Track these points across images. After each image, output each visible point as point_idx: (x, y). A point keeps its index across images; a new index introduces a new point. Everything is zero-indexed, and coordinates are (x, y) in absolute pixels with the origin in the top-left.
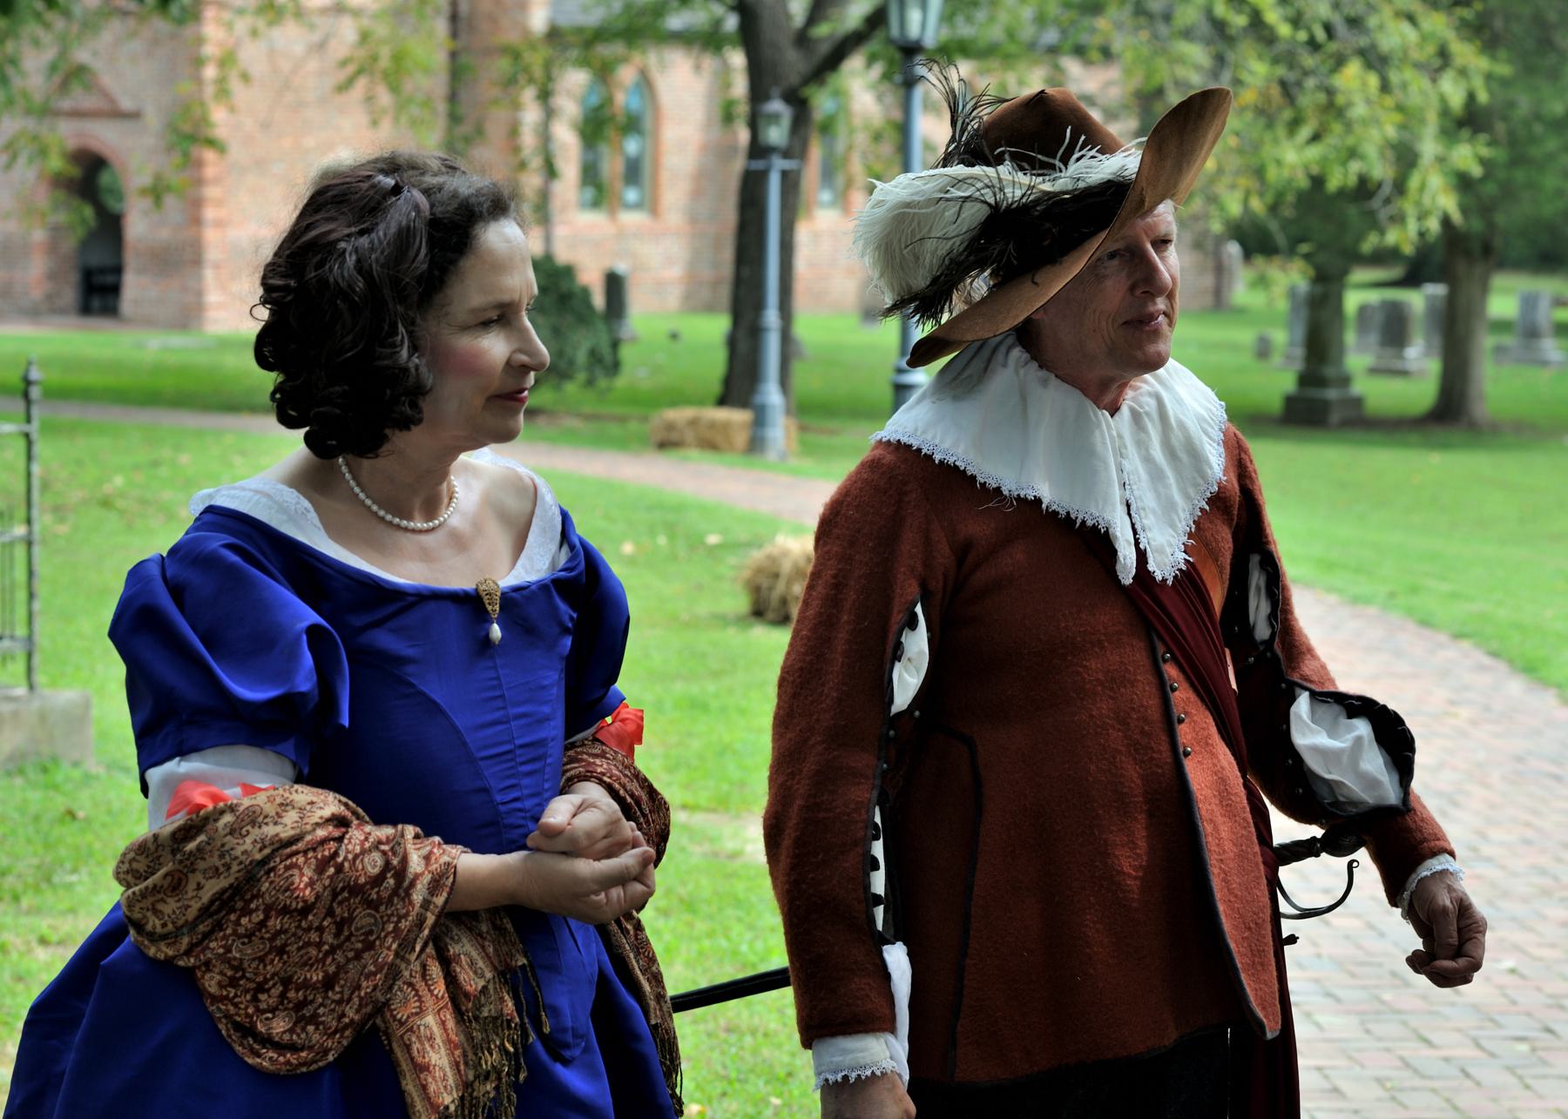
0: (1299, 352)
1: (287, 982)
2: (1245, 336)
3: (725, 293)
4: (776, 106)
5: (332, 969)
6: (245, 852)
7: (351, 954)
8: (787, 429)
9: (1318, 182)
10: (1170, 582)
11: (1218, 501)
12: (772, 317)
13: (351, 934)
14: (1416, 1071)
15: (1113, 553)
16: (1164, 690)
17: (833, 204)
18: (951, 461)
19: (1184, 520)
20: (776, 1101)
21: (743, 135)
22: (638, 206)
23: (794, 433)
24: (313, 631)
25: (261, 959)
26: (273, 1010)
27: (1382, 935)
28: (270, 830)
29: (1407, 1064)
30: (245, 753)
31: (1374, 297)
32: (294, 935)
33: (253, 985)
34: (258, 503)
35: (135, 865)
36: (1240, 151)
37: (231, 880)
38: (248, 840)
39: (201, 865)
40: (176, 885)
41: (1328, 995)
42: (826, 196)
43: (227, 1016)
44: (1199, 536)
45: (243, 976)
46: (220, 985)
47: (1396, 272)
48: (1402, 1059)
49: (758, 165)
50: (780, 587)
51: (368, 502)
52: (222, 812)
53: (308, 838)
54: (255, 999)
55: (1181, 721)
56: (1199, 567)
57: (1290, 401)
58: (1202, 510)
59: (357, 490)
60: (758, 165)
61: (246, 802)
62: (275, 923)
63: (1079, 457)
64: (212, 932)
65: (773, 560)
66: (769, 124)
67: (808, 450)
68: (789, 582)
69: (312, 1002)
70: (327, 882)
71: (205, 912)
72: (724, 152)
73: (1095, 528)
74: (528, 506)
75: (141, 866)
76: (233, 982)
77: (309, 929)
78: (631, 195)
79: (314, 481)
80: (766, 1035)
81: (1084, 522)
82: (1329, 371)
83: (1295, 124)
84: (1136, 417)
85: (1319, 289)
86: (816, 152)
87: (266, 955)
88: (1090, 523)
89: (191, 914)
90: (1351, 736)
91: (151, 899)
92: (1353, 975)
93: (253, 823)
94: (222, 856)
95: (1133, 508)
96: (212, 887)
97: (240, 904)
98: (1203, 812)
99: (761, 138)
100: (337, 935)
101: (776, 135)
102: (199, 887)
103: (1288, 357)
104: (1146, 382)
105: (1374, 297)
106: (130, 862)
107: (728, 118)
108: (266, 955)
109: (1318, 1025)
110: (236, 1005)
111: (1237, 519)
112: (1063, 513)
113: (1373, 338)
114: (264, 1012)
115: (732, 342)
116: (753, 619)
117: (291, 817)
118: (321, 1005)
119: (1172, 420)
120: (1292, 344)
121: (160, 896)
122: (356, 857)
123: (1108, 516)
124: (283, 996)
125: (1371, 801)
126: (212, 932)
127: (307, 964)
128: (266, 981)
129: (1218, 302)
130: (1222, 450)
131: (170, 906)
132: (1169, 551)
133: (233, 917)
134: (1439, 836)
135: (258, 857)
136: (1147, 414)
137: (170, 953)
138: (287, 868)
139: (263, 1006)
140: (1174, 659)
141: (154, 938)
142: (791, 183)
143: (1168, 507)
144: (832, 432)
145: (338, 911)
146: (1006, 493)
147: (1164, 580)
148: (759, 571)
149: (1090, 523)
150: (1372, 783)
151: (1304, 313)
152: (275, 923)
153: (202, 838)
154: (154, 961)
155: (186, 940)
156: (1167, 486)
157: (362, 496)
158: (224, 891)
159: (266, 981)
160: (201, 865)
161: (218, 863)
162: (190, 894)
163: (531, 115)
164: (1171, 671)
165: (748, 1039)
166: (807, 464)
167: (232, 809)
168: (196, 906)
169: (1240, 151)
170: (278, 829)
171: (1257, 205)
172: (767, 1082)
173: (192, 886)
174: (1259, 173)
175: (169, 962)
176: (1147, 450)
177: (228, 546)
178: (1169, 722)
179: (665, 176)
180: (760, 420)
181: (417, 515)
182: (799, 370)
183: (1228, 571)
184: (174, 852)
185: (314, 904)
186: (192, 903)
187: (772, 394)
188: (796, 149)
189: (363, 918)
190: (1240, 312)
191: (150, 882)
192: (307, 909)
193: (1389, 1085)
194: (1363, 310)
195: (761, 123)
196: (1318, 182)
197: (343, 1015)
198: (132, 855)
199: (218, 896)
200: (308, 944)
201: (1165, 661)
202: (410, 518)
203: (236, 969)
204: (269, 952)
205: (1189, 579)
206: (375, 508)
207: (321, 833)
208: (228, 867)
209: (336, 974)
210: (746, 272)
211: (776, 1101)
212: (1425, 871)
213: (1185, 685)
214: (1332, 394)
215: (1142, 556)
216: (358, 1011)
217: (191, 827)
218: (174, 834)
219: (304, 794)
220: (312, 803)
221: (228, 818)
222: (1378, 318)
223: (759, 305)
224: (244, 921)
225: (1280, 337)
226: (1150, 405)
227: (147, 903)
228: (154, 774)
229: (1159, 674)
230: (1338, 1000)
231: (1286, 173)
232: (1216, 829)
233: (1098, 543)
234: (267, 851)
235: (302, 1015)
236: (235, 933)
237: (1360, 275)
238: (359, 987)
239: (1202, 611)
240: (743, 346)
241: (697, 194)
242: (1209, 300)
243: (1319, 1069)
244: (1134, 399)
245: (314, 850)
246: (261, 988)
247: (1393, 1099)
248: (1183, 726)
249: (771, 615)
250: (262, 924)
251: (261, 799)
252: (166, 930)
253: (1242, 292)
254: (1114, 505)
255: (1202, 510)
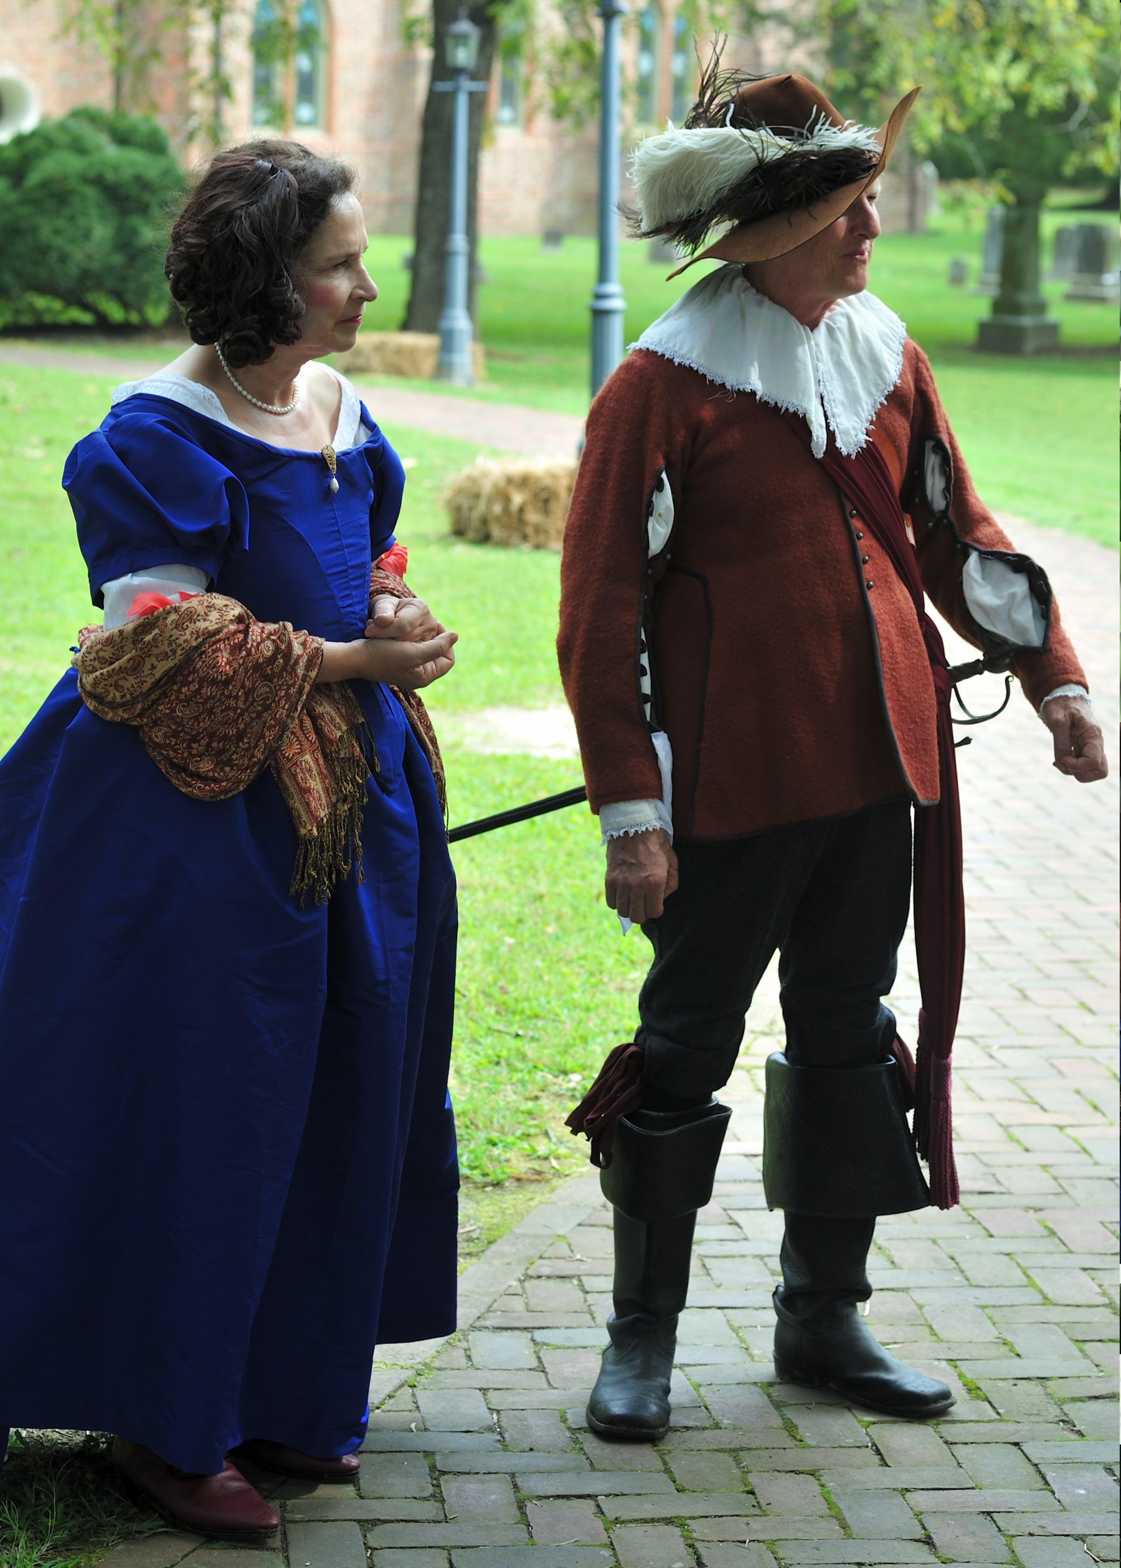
0: (994, 278)
1: (212, 735)
2: (939, 261)
3: (407, 217)
4: (464, 26)
5: (242, 726)
6: (185, 641)
7: (253, 715)
8: (474, 353)
9: (1021, 100)
10: (853, 457)
11: (895, 398)
12: (459, 241)
13: (254, 700)
14: (1075, 924)
15: (809, 433)
16: (852, 539)
17: (513, 121)
18: (687, 363)
19: (867, 408)
20: (509, 940)
21: (425, 54)
22: (311, 123)
23: (481, 360)
24: (229, 481)
25: (196, 719)
26: (201, 755)
27: (1050, 815)
28: (202, 625)
29: (1066, 918)
30: (178, 570)
31: (1071, 220)
32: (219, 700)
33: (189, 737)
34: (176, 391)
35: (101, 654)
36: (937, 72)
37: (176, 661)
38: (188, 632)
39: (155, 651)
40: (136, 667)
41: (999, 862)
42: (506, 114)
43: (167, 759)
44: (880, 424)
45: (183, 731)
46: (165, 736)
47: (1097, 194)
48: (1063, 914)
49: (443, 86)
50: (481, 507)
51: (245, 393)
52: (169, 613)
53: (226, 630)
54: (189, 747)
55: (865, 562)
56: (879, 447)
57: (984, 328)
58: (881, 404)
59: (236, 384)
60: (443, 86)
61: (185, 605)
62: (207, 691)
63: (782, 361)
64: (159, 699)
65: (473, 480)
66: (457, 45)
67: (495, 376)
68: (490, 502)
69: (228, 750)
70: (241, 661)
71: (156, 684)
72: (404, 68)
73: (795, 413)
74: (336, 399)
75: (107, 654)
76: (175, 734)
77: (230, 696)
78: (305, 112)
79: (208, 374)
80: (496, 890)
81: (787, 409)
82: (1025, 298)
83: (993, 43)
84: (830, 330)
85: (1014, 214)
86: (498, 68)
87: (200, 715)
88: (791, 410)
89: (146, 687)
90: (1007, 592)
91: (115, 678)
92: (1022, 847)
93: (191, 620)
94: (170, 644)
95: (826, 399)
96: (162, 667)
97: (180, 678)
98: (881, 631)
99: (449, 60)
100: (245, 702)
101: (463, 56)
102: (153, 667)
103: (983, 283)
104: (839, 305)
105: (1071, 220)
106: (97, 652)
107: (409, 35)
108: (200, 715)
109: (989, 888)
110: (175, 751)
111: (913, 412)
112: (772, 403)
113: (1071, 263)
114: (195, 756)
115: (413, 265)
116: (453, 539)
117: (214, 616)
118: (234, 753)
119: (860, 337)
120: (987, 269)
121: (122, 675)
122: (259, 644)
123: (805, 405)
124: (209, 745)
125: (1021, 644)
126: (159, 699)
127: (227, 723)
128: (198, 734)
129: (912, 225)
130: (900, 359)
131: (130, 682)
132: (853, 433)
133: (175, 688)
134: (1078, 671)
135: (194, 644)
136: (839, 329)
137: (126, 716)
138: (214, 651)
139: (195, 752)
140: (860, 515)
141: (113, 706)
142: (478, 104)
143: (853, 400)
144: (517, 359)
145: (247, 683)
146: (729, 387)
147: (849, 455)
148: (460, 491)
149: (791, 410)
150: (1022, 631)
151: (999, 238)
152: (207, 691)
153: (156, 631)
154: (111, 723)
155: (140, 706)
156: (854, 385)
157: (240, 388)
158: (171, 669)
159: (198, 734)
160: (155, 651)
161: (168, 650)
162: (146, 672)
163: (203, 33)
164: (857, 524)
165: (480, 895)
166: (494, 389)
167: (176, 610)
168: (150, 681)
169: (937, 72)
170: (207, 624)
171: (954, 123)
172: (501, 927)
173: (148, 666)
174: (956, 93)
175: (123, 724)
176: (838, 356)
177: (158, 422)
178: (856, 564)
179: (339, 92)
180: (447, 345)
181: (277, 402)
182: (484, 295)
183: (906, 451)
184: (134, 642)
185: (233, 677)
186: (148, 679)
187: (459, 320)
188: (481, 72)
189: (263, 690)
190: (936, 234)
191: (116, 665)
192: (228, 681)
193: (1049, 933)
194: (1061, 234)
195: (449, 43)
196: (1021, 100)
197: (254, 756)
198: (99, 646)
199: (166, 674)
200: (228, 708)
201: (852, 516)
202: (272, 404)
203: (178, 724)
204: (202, 713)
205: (869, 453)
206: (249, 397)
207: (233, 627)
208: (174, 652)
209: (245, 730)
210: (429, 194)
211: (509, 940)
212: (1058, 693)
213: (869, 535)
214: (1027, 321)
215: (831, 436)
216: (263, 753)
217: (148, 624)
218: (135, 629)
219: (219, 600)
220: (226, 606)
221: (173, 617)
222: (1076, 243)
223: (446, 230)
224: (184, 690)
225: (974, 262)
226: (842, 323)
227: (112, 681)
228: (111, 588)
229: (848, 526)
230: (1007, 867)
231: (986, 93)
232: (891, 645)
233: (799, 424)
234: (200, 640)
235: (222, 759)
236: (177, 698)
237: (1057, 197)
238: (263, 736)
239: (877, 472)
240: (426, 270)
241: (373, 110)
242: (902, 223)
243: (988, 921)
244: (830, 318)
245: (228, 639)
246: (194, 739)
247: (1053, 945)
248: (866, 566)
249: (471, 534)
250: (198, 691)
251: (194, 602)
252: (124, 700)
253: (935, 216)
254: (810, 396)
255: (881, 404)
